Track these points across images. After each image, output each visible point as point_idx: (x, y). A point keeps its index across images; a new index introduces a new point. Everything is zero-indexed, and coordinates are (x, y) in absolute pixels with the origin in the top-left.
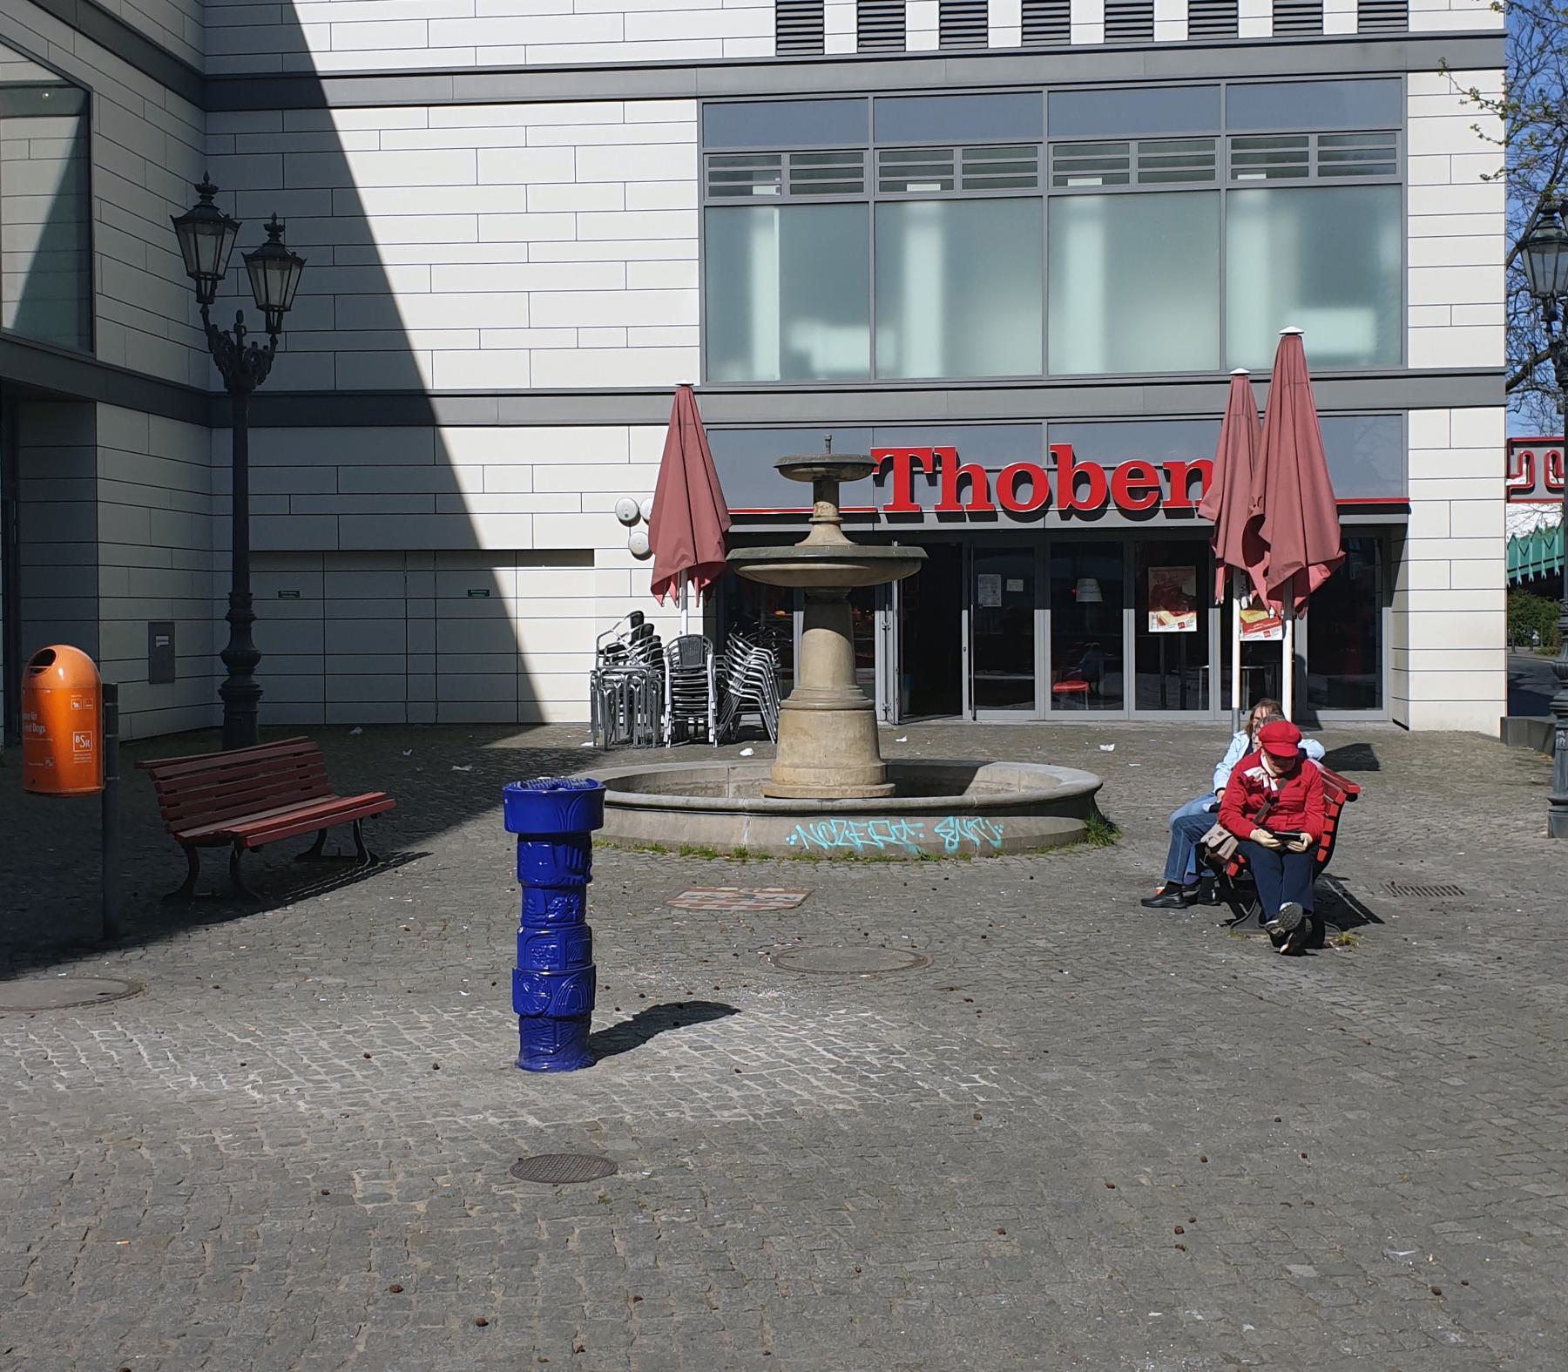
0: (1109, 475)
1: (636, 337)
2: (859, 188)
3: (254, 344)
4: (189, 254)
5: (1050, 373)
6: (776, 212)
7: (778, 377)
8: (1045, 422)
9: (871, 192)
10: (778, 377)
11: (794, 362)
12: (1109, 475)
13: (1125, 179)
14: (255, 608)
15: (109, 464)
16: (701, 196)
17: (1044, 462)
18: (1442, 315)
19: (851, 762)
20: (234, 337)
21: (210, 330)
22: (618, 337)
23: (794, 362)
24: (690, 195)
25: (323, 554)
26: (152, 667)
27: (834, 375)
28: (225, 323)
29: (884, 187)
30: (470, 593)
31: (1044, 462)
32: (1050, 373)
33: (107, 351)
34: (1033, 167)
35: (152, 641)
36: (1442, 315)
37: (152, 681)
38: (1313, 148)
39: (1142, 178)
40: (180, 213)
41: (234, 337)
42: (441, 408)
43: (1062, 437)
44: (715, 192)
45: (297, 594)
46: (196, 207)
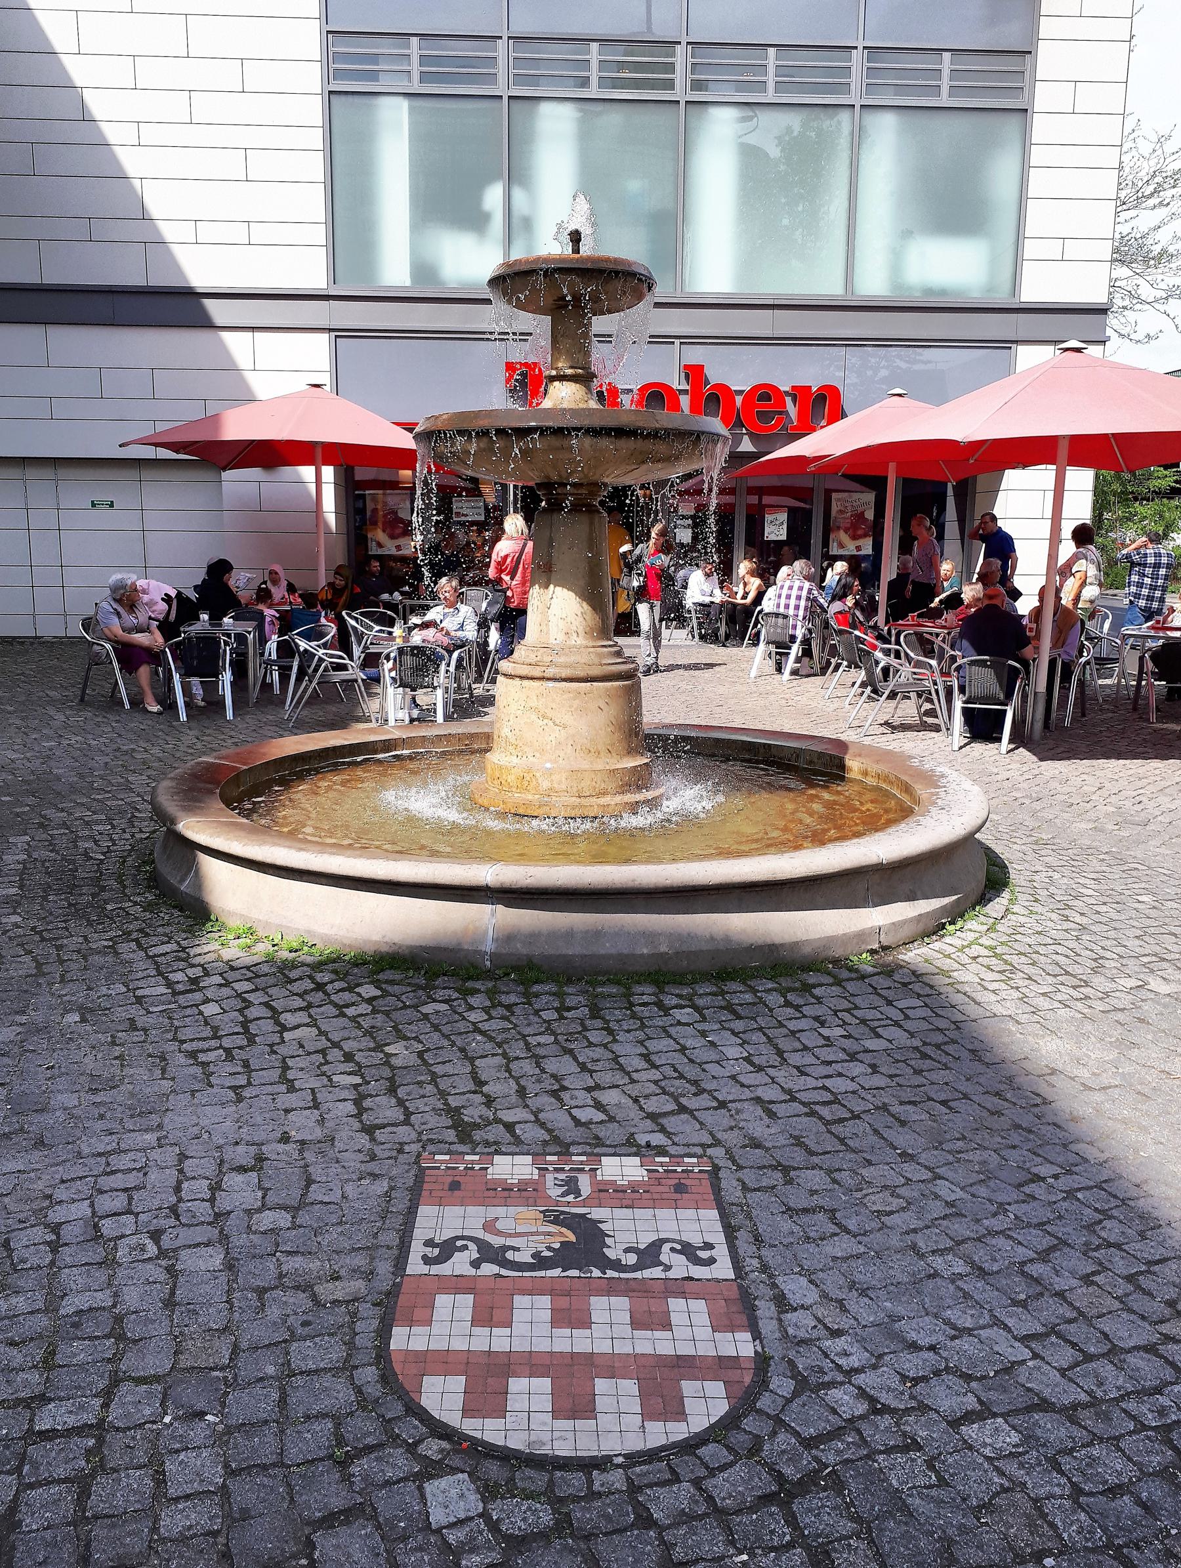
0: (739, 400)
1: (260, 233)
2: (669, 85)
5: (687, 290)
7: (408, 283)
8: (677, 342)
9: (680, 92)
10: (408, 283)
11: (423, 270)
12: (739, 400)
13: (585, 82)
16: (327, 78)
17: (677, 382)
18: (1074, 250)
22: (239, 233)
23: (423, 270)
24: (312, 78)
27: (929, 291)
29: (519, 79)
30: (93, 505)
31: (677, 382)
32: (687, 290)
34: (670, 68)
36: (1074, 250)
38: (680, 58)
39: (424, 77)
42: (217, 310)
43: (695, 355)
44: (339, 74)
45: (112, 505)
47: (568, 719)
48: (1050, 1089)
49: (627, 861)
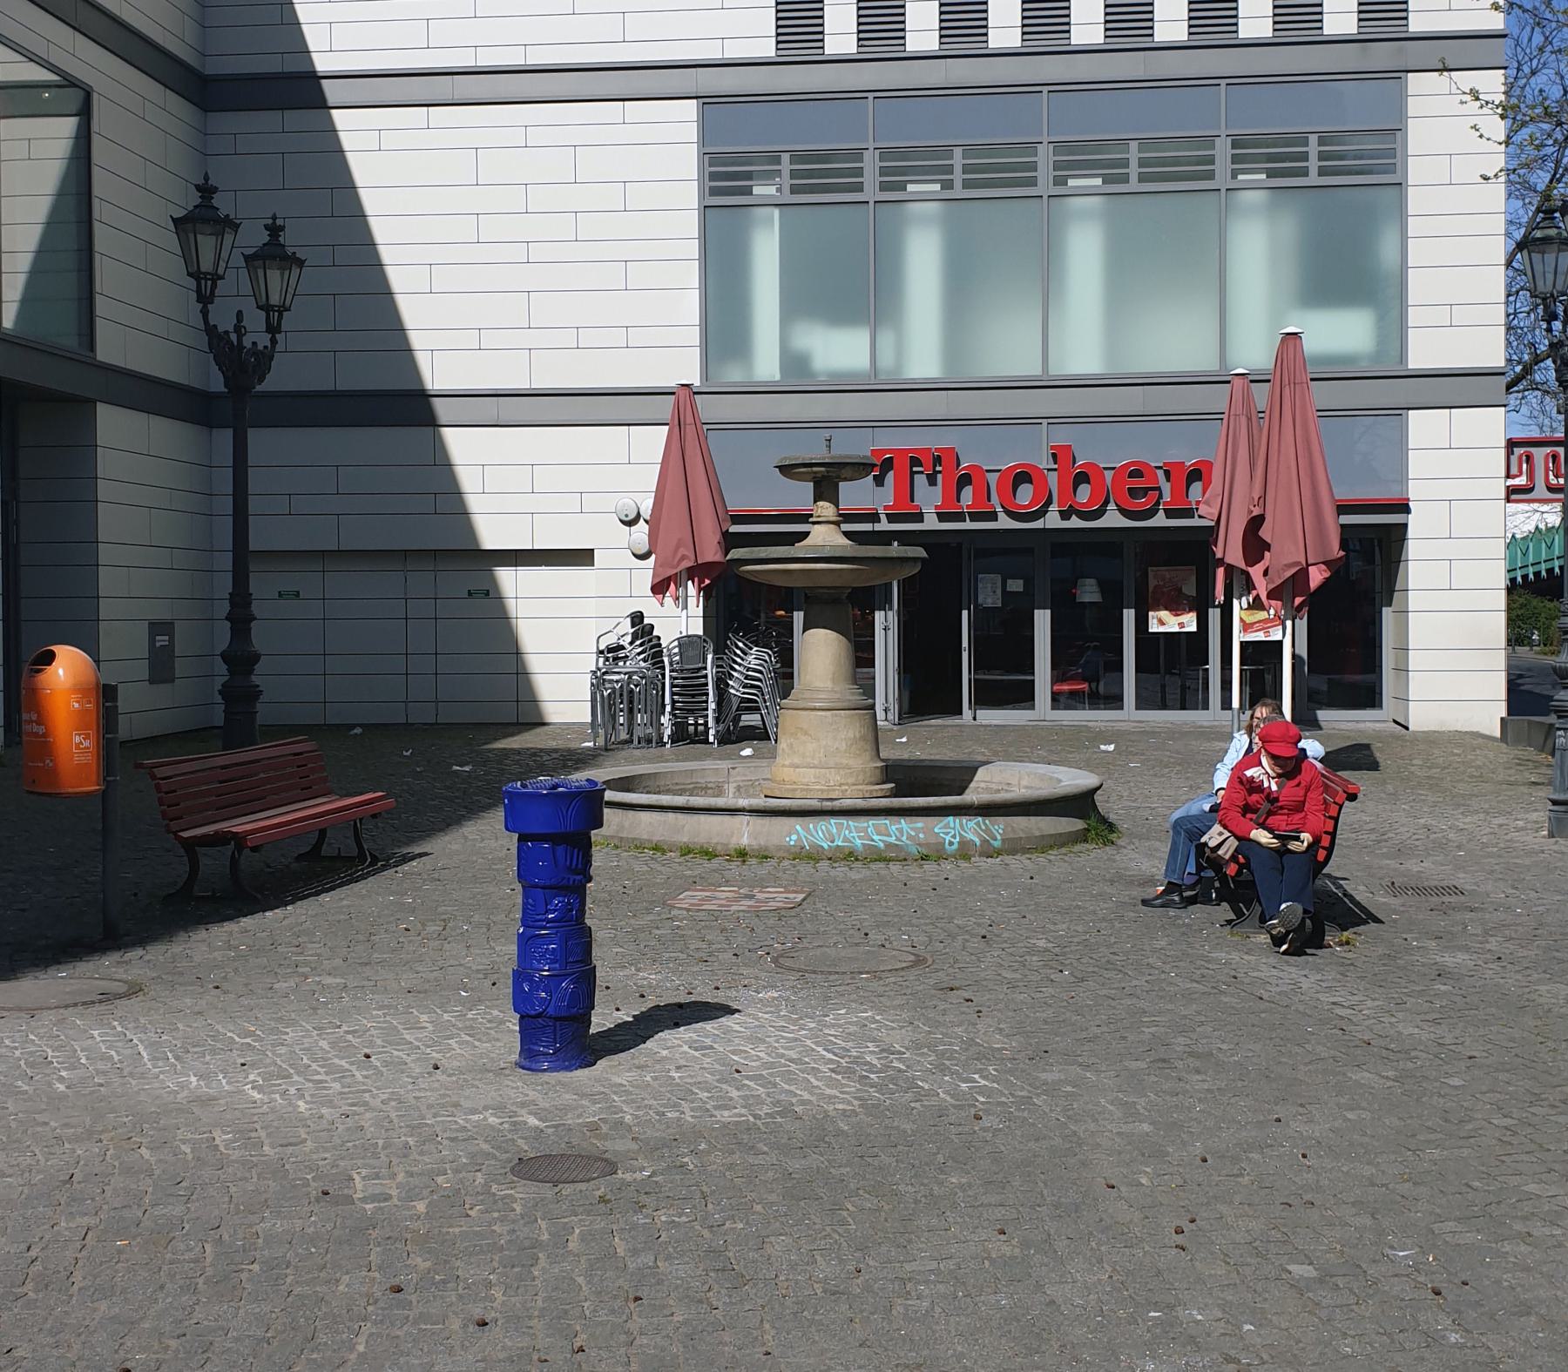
0: (1109, 475)
1: (636, 337)
2: (859, 188)
3: (254, 344)
4: (189, 254)
5: (1050, 373)
6: (776, 212)
7: (778, 377)
8: (1045, 422)
9: (871, 192)
10: (778, 377)
11: (794, 362)
12: (1109, 475)
13: (1125, 179)
14: (255, 608)
15: (109, 464)
16: (701, 196)
17: (1044, 462)
18: (1442, 315)
20: (234, 337)
21: (210, 330)
22: (618, 337)
23: (794, 362)
24: (690, 195)
25: (323, 554)
26: (152, 667)
28: (225, 323)
29: (884, 187)
30: (470, 593)
31: (1044, 462)
32: (1050, 373)
33: (107, 351)
34: (1033, 167)
35: (152, 641)
36: (1442, 315)
37: (152, 681)
38: (1313, 148)
39: (1142, 178)
40: (180, 213)
41: (234, 337)
43: (1062, 437)
44: (715, 192)
46: (196, 207)
47: (851, 762)
48: (184, 642)
49: (628, 791)
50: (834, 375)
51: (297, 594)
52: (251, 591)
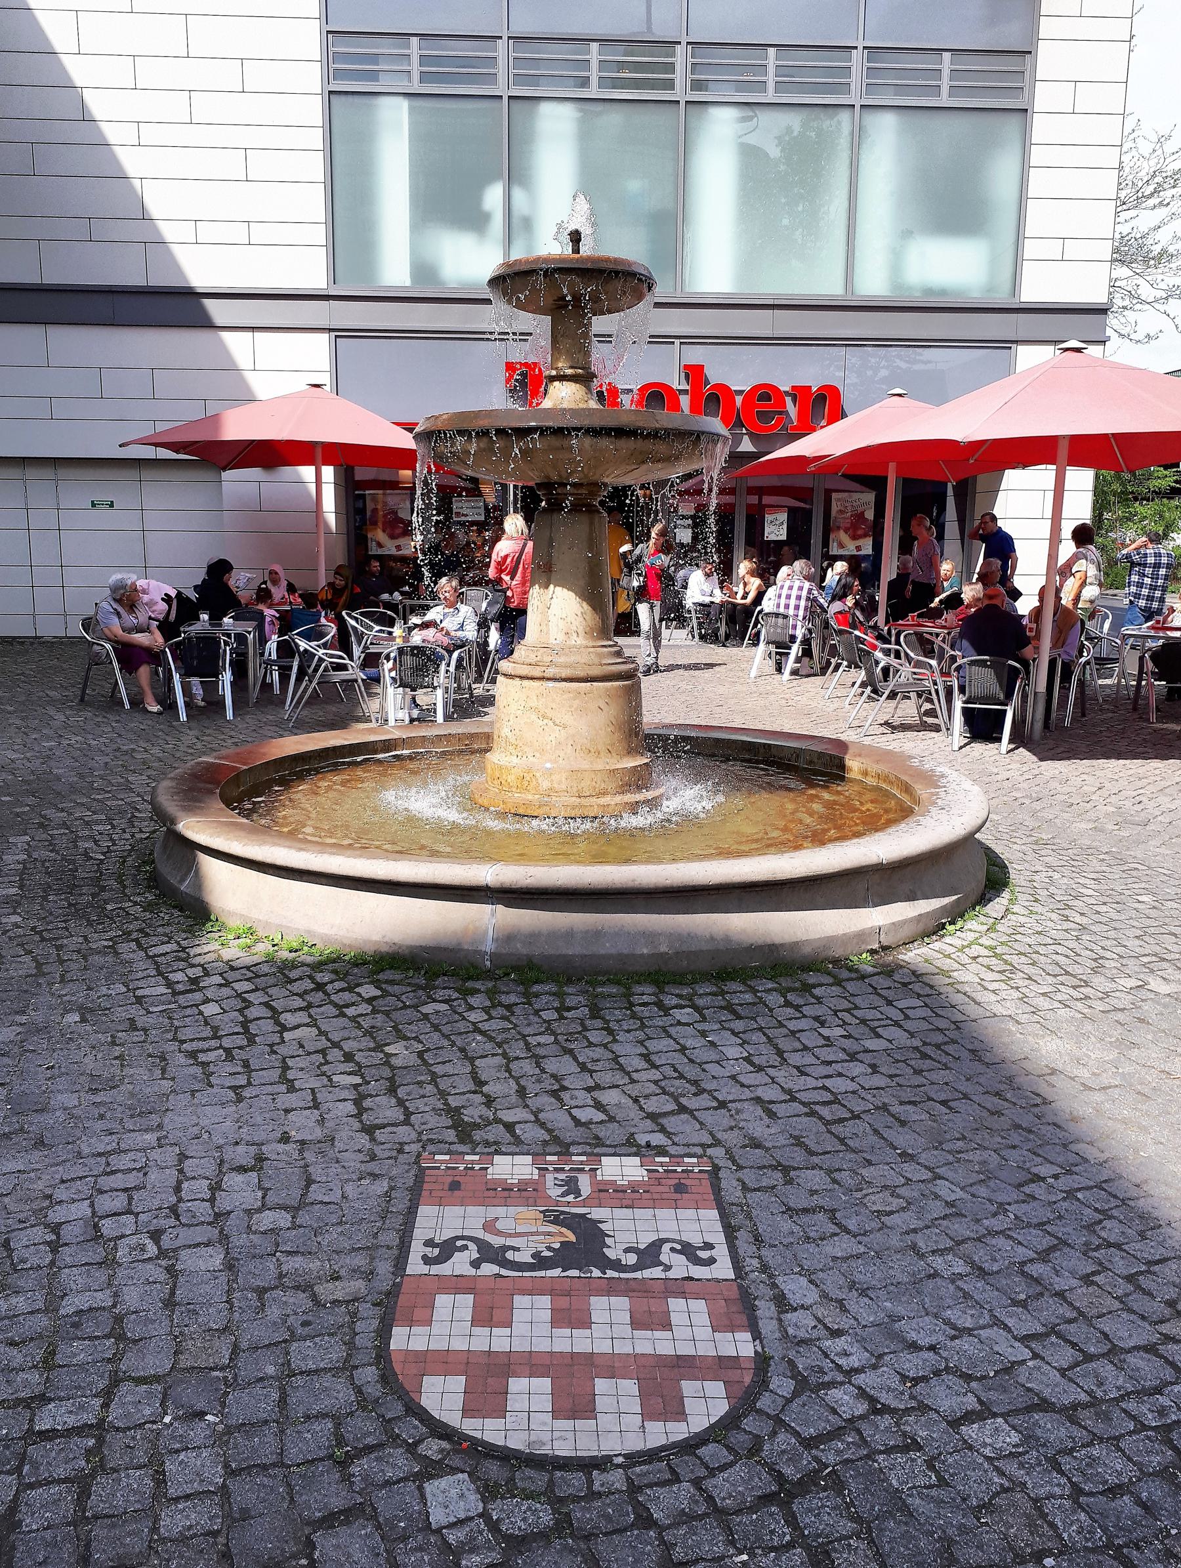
0: (739, 400)
1: (260, 233)
2: (669, 85)
5: (687, 290)
7: (408, 283)
8: (677, 342)
9: (680, 92)
10: (408, 283)
11: (423, 270)
12: (739, 400)
13: (585, 82)
16: (327, 78)
17: (677, 382)
18: (1074, 250)
19: (568, 719)
22: (239, 233)
23: (423, 270)
24: (312, 78)
29: (519, 79)
30: (93, 505)
31: (677, 382)
32: (687, 290)
34: (670, 68)
36: (1074, 250)
38: (680, 58)
39: (424, 77)
43: (695, 355)
44: (339, 74)
50: (929, 291)
51: (112, 505)
52: (996, 512)
